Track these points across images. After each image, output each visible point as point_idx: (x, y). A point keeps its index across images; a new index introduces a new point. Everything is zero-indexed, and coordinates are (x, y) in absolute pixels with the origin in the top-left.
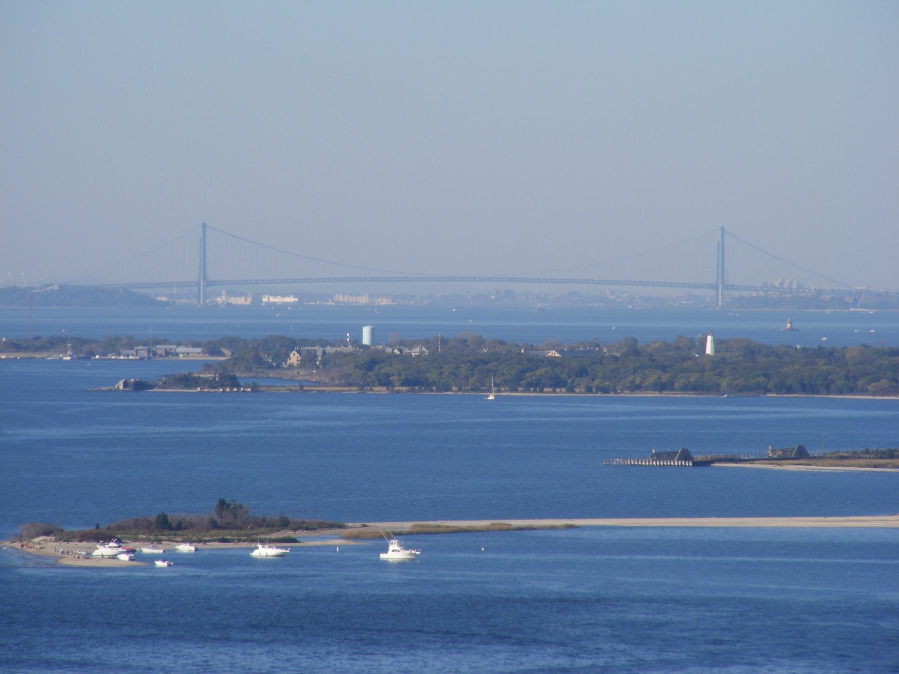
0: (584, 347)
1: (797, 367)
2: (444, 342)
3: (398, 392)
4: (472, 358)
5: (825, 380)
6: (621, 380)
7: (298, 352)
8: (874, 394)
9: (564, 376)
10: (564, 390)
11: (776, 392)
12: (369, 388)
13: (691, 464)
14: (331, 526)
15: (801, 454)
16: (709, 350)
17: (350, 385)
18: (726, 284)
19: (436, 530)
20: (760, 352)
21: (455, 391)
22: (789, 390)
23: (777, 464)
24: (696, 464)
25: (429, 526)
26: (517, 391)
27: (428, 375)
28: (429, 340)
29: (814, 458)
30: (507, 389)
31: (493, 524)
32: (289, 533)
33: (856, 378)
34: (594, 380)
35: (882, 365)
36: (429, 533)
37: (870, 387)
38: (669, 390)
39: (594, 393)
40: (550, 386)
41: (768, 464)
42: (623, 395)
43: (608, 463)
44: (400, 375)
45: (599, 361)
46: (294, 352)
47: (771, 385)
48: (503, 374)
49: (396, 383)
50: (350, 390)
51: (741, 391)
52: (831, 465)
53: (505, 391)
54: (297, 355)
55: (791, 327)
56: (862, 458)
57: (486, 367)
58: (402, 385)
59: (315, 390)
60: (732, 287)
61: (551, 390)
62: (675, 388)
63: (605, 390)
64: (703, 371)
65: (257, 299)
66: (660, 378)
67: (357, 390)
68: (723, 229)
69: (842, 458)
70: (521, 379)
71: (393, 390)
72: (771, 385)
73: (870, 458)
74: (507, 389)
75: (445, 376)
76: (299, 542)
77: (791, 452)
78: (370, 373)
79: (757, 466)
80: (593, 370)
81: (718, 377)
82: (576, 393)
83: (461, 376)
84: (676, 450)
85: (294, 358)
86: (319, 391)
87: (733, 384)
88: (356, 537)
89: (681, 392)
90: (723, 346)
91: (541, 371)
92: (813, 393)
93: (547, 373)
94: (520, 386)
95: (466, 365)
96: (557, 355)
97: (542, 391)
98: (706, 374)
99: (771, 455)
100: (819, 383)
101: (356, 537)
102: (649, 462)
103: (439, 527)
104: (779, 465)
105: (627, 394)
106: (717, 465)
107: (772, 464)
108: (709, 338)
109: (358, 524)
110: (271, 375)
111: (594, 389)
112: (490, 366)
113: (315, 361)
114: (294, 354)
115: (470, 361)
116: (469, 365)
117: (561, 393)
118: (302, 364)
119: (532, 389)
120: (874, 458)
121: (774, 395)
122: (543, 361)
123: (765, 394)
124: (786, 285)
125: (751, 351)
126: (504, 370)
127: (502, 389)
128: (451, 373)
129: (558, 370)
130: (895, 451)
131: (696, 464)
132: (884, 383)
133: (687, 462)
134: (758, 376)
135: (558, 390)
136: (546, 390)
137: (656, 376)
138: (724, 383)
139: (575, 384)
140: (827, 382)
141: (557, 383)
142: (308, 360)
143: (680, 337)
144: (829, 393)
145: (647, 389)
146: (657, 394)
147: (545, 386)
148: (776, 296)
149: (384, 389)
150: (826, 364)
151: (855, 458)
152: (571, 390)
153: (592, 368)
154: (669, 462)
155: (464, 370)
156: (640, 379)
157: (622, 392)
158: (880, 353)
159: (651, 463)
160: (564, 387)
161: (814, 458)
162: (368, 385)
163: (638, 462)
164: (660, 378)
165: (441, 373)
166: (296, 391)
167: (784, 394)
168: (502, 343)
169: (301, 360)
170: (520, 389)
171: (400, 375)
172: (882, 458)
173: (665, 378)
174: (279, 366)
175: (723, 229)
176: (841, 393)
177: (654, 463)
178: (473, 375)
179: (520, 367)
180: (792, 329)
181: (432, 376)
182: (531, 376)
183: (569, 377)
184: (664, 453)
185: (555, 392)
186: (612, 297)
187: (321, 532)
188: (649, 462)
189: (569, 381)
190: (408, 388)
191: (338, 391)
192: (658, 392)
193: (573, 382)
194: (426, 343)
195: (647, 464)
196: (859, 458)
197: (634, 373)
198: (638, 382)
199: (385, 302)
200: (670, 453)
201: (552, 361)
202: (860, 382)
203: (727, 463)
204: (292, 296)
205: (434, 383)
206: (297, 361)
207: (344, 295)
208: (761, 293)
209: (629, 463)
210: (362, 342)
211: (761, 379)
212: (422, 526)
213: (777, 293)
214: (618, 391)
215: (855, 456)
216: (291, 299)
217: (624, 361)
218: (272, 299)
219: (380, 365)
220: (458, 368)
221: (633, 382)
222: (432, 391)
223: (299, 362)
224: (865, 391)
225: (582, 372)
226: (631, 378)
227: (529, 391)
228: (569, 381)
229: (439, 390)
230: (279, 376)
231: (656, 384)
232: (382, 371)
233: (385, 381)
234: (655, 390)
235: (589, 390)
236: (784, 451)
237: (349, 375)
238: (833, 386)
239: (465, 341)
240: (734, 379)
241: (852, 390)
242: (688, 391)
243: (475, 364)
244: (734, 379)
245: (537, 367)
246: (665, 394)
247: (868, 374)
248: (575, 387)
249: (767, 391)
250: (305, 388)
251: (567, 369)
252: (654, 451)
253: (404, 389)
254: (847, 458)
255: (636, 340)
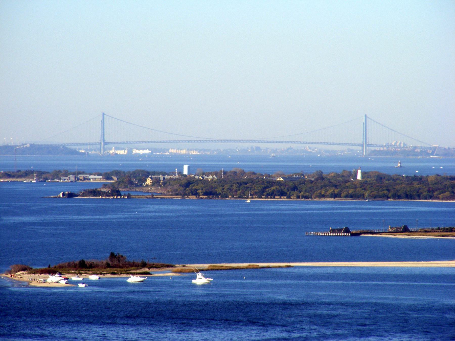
0: (295, 176)
1: (403, 186)
2: (225, 173)
3: (202, 198)
4: (239, 181)
5: (418, 192)
6: (314, 192)
7: (151, 178)
8: (443, 199)
9: (285, 190)
10: (285, 197)
11: (393, 199)
12: (187, 196)
13: (350, 235)
14: (168, 266)
15: (406, 230)
16: (359, 177)
17: (177, 195)
18: (367, 143)
19: (221, 268)
20: (385, 178)
21: (230, 198)
22: (399, 197)
23: (393, 235)
24: (353, 235)
25: (217, 266)
26: (261, 198)
27: (217, 190)
28: (217, 172)
29: (412, 232)
30: (257, 197)
31: (250, 265)
32: (146, 270)
33: (433, 191)
34: (300, 192)
35: (446, 184)
36: (217, 270)
37: (440, 196)
38: (339, 198)
39: (301, 199)
40: (278, 195)
41: (389, 235)
42: (315, 200)
43: (307, 234)
44: (202, 190)
45: (303, 183)
46: (149, 178)
47: (390, 195)
48: (255, 189)
49: (201, 194)
50: (177, 197)
51: (375, 198)
52: (421, 235)
53: (256, 198)
54: (150, 179)
55: (401, 165)
56: (436, 232)
57: (246, 186)
58: (204, 195)
59: (159, 197)
60: (371, 145)
61: (279, 197)
62: (342, 196)
63: (306, 197)
64: (356, 188)
65: (130, 151)
66: (334, 191)
67: (181, 197)
68: (366, 116)
69: (426, 232)
70: (264, 192)
71: (199, 197)
72: (390, 195)
73: (440, 232)
74: (257, 197)
75: (225, 190)
76: (151, 274)
77: (401, 229)
78: (187, 189)
79: (383, 236)
80: (300, 187)
81: (363, 191)
82: (292, 199)
83: (233, 190)
84: (342, 228)
85: (149, 181)
86: (161, 198)
87: (371, 194)
88: (180, 272)
89: (345, 199)
90: (366, 175)
91: (274, 188)
92: (412, 199)
93: (277, 189)
94: (263, 195)
95: (236, 185)
96: (282, 180)
97: (274, 198)
98: (358, 189)
99: (390, 230)
100: (414, 194)
101: (180, 272)
102: (329, 234)
103: (222, 266)
104: (395, 235)
105: (317, 200)
106: (363, 235)
107: (391, 235)
108: (359, 171)
109: (181, 265)
110: (137, 190)
111: (300, 197)
112: (248, 185)
113: (159, 183)
114: (149, 179)
115: (238, 183)
116: (238, 185)
117: (284, 199)
118: (153, 184)
119: (269, 197)
120: (442, 232)
121: (392, 200)
122: (275, 183)
123: (387, 199)
124: (398, 144)
125: (380, 178)
126: (255, 187)
127: (254, 197)
128: (228, 189)
129: (282, 187)
130: (453, 228)
131: (353, 235)
132: (447, 194)
133: (348, 234)
134: (384, 190)
135: (282, 197)
136: (276, 197)
137: (332, 190)
138: (367, 194)
139: (291, 194)
140: (419, 193)
141: (282, 194)
142: (156, 182)
143: (344, 170)
144: (420, 199)
145: (327, 197)
146: (332, 200)
147: (276, 195)
148: (393, 150)
149: (195, 197)
150: (418, 184)
151: (433, 232)
152: (289, 197)
153: (300, 186)
154: (338, 234)
155: (235, 187)
156: (324, 192)
157: (315, 198)
158: (446, 179)
159: (329, 234)
160: (285, 196)
161: (412, 232)
162: (186, 195)
163: (323, 234)
164: (334, 191)
165: (223, 189)
166: (150, 198)
167: (397, 199)
168: (254, 173)
169: (152, 182)
170: (263, 197)
171: (202, 190)
172: (446, 232)
173: (336, 191)
174: (141, 185)
175: (366, 116)
176: (426, 199)
177: (331, 234)
178: (239, 190)
179: (263, 186)
180: (401, 166)
181: (219, 190)
182: (269, 190)
183: (288, 191)
184: (336, 229)
185: (281, 198)
186: (310, 150)
187: (162, 269)
188: (329, 234)
189: (288, 193)
190: (206, 196)
191: (171, 198)
192: (333, 198)
193: (290, 193)
194: (216, 173)
195: (328, 235)
196: (435, 232)
197: (321, 189)
198: (323, 193)
199: (195, 153)
200: (339, 229)
201: (279, 183)
202: (435, 194)
203: (368, 234)
204: (148, 150)
205: (220, 194)
206: (151, 182)
207: (174, 149)
208: (385, 148)
209: (318, 234)
210: (183, 172)
211: (385, 192)
212: (214, 266)
213: (393, 148)
214: (313, 198)
215: (433, 231)
216: (147, 151)
217: (316, 183)
218: (138, 151)
219: (192, 185)
220: (232, 186)
221: (320, 193)
222: (219, 198)
223: (151, 183)
224: (438, 198)
225: (295, 188)
226: (319, 191)
227: (267, 198)
228: (288, 193)
229: (222, 197)
230: (141, 190)
231: (332, 194)
232: (194, 188)
233: (195, 193)
234: (331, 197)
235: (298, 197)
236: (397, 228)
237: (177, 190)
238: (421, 195)
239: (235, 172)
240: (371, 192)
241: (431, 197)
242: (348, 198)
243: (240, 184)
244: (371, 192)
245: (272, 186)
246: (337, 200)
247: (439, 189)
248: (291, 196)
249: (388, 198)
250: (155, 197)
251: (287, 187)
252: (331, 228)
253: (205, 197)
254: (429, 232)
255: (322, 172)
